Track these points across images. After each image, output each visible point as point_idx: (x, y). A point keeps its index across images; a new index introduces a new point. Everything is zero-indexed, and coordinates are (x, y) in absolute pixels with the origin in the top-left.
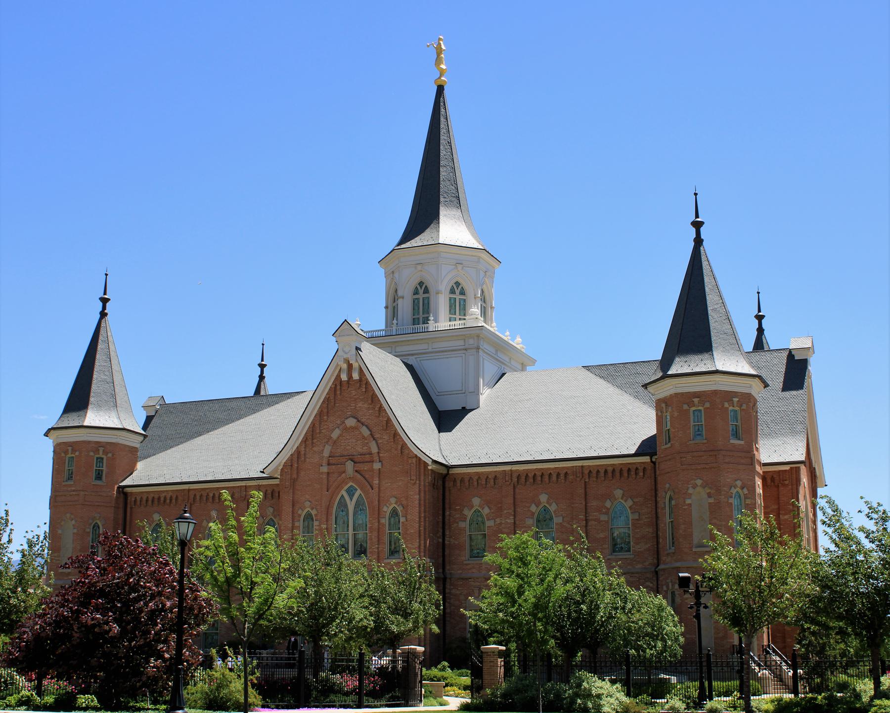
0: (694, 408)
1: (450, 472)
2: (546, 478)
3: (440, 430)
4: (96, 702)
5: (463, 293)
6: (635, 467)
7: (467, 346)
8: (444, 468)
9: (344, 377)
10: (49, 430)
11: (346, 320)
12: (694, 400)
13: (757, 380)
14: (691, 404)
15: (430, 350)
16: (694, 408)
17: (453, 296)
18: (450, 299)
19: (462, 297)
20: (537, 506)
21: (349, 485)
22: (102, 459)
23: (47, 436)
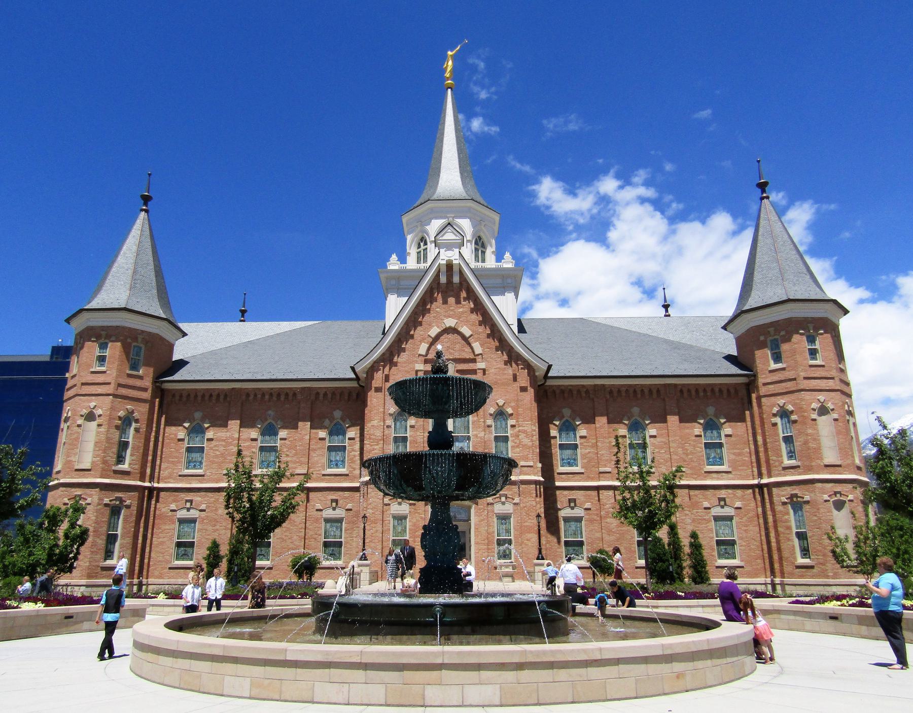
0: (771, 338)
2: (282, 398)
3: (53, 347)
4: (738, 586)
6: (216, 393)
9: (443, 279)
12: (769, 330)
13: (165, 323)
14: (135, 339)
16: (771, 338)
20: (331, 422)
22: (140, 348)
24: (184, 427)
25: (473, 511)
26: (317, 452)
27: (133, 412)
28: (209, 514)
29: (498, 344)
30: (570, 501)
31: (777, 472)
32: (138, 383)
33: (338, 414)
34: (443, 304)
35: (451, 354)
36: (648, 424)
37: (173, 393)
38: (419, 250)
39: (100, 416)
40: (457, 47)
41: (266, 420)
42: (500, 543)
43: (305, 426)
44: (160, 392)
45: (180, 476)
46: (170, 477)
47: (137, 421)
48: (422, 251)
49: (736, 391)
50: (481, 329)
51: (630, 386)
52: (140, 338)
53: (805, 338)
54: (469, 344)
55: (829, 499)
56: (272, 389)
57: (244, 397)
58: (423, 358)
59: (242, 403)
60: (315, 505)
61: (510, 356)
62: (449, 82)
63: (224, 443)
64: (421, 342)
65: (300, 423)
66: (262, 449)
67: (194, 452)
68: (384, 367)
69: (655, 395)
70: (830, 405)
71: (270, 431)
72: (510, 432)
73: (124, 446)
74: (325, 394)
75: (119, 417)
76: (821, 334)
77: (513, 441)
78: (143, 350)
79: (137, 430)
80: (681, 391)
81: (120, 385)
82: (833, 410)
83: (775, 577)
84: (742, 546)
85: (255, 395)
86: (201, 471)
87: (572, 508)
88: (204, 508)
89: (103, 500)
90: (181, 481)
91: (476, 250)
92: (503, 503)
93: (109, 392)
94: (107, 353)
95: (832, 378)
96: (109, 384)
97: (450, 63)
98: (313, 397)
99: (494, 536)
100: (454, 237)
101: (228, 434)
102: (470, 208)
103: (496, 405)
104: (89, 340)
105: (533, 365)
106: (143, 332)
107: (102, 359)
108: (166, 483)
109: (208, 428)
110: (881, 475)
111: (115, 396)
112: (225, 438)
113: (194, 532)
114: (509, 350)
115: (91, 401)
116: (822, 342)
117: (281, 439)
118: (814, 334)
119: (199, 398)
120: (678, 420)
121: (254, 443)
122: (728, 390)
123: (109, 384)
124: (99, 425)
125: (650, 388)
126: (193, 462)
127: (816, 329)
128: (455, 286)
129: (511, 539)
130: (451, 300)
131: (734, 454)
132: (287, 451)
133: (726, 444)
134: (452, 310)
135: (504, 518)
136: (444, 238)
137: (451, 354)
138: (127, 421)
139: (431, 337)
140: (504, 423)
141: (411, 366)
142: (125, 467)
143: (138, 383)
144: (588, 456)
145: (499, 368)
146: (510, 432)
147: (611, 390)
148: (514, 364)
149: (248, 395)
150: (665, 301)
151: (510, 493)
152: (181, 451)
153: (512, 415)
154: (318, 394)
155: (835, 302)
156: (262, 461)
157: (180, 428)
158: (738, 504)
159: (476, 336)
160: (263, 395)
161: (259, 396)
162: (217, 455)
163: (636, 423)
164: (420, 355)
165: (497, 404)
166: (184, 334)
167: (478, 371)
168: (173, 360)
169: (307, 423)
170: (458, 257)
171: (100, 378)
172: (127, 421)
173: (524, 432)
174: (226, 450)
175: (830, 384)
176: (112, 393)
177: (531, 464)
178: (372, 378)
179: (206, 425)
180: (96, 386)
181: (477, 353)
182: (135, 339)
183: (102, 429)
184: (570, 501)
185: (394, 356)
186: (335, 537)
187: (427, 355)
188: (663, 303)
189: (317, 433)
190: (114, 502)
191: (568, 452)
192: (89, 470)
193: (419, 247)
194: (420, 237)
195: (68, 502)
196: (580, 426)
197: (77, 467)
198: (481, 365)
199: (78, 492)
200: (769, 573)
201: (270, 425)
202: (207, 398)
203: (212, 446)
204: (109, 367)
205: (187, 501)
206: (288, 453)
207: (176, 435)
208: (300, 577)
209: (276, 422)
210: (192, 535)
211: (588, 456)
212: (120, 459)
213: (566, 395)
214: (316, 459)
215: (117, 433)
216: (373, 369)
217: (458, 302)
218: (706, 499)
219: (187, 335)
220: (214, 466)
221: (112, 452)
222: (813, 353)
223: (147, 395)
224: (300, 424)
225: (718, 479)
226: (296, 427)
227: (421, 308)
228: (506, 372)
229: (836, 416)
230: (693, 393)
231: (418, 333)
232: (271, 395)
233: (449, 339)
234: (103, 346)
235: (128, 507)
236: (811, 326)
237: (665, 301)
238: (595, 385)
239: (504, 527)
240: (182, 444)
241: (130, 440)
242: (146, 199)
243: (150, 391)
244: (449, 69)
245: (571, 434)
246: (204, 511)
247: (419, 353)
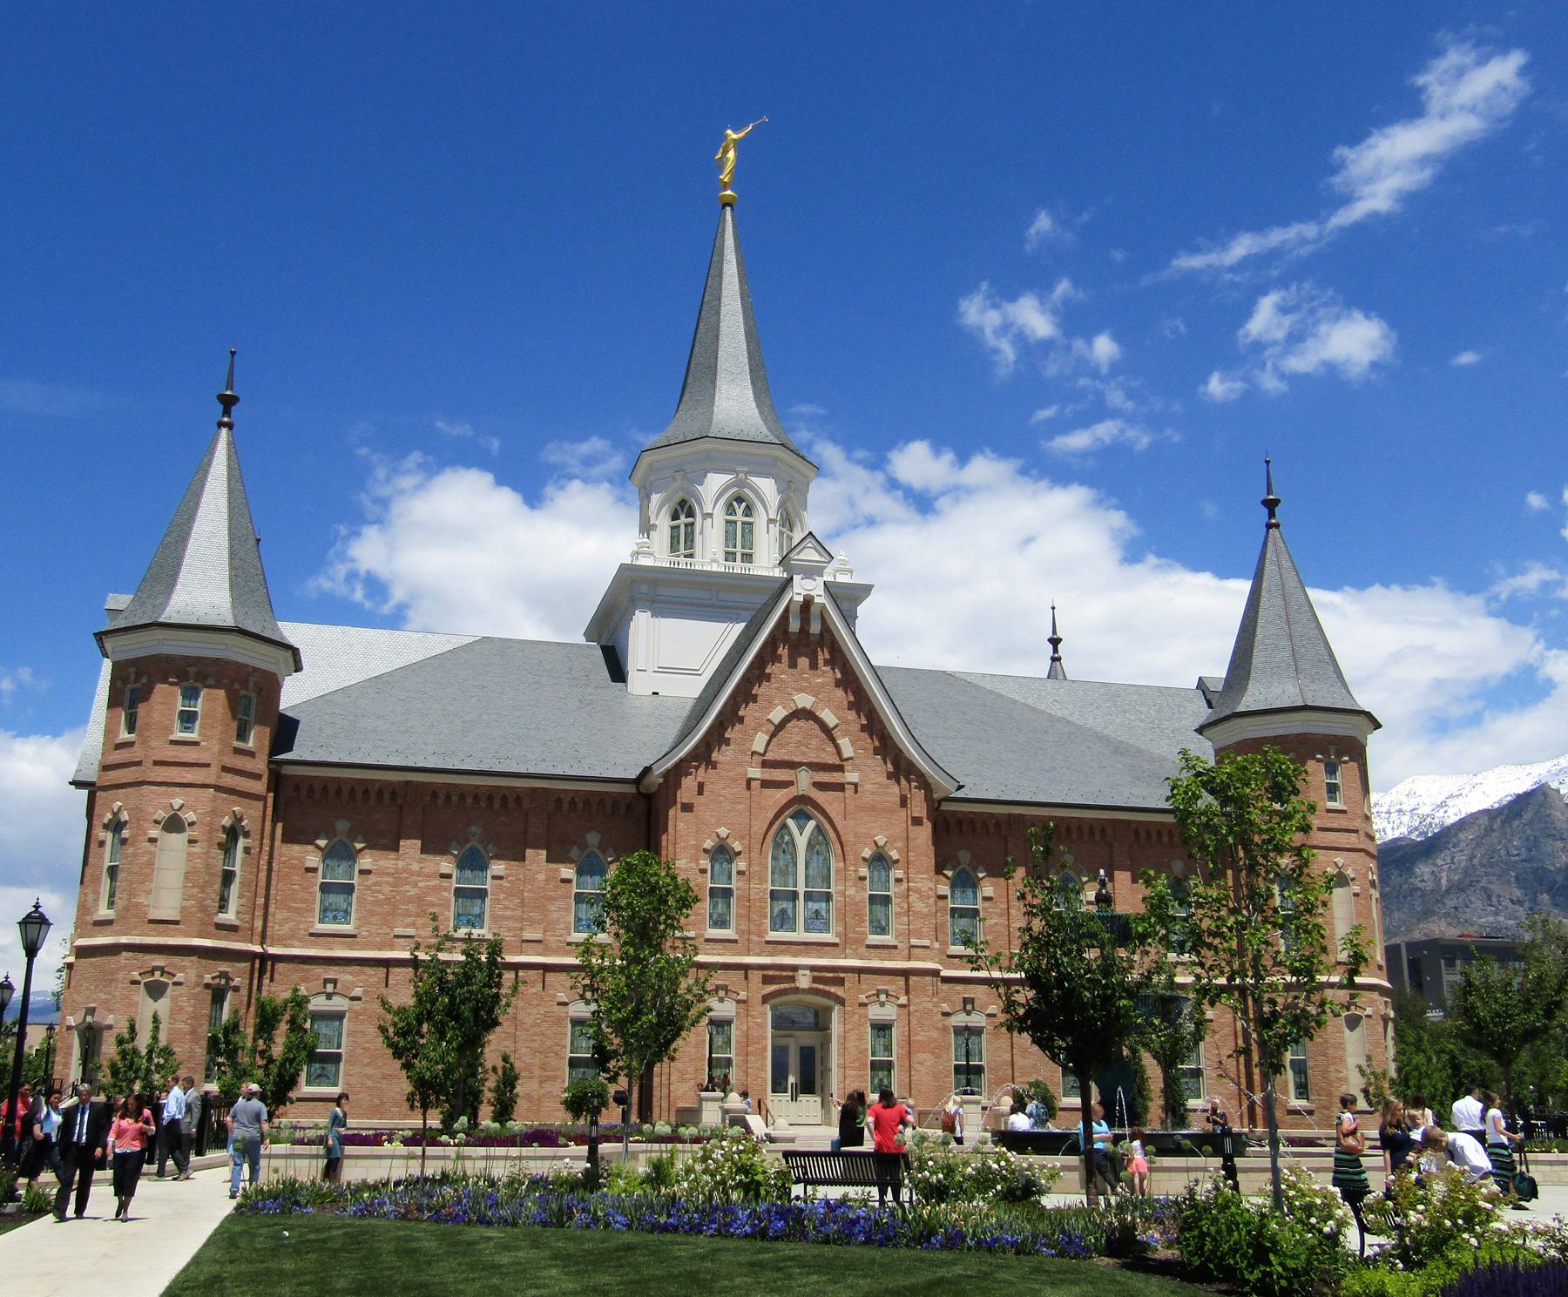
2: (497, 805)
6: (377, 787)
24: (318, 847)
25: (835, 1016)
26: (557, 904)
27: (241, 819)
28: (368, 1006)
29: (877, 743)
30: (966, 1001)
33: (593, 838)
34: (790, 667)
35: (803, 753)
36: (1086, 883)
37: (297, 782)
38: (676, 522)
39: (192, 824)
40: (748, 126)
41: (467, 841)
42: (875, 1066)
43: (537, 857)
44: (277, 780)
45: (311, 935)
46: (292, 937)
47: (247, 835)
48: (682, 527)
50: (852, 715)
51: (360, 781)
52: (252, 680)
53: (1322, 766)
54: (833, 740)
58: (761, 759)
59: (424, 809)
60: (556, 996)
61: (896, 764)
62: (729, 192)
63: (390, 879)
64: (756, 730)
65: (528, 850)
66: (459, 893)
67: (333, 893)
68: (697, 768)
69: (1098, 837)
70: (1350, 873)
71: (473, 862)
72: (893, 890)
73: (228, 877)
74: (573, 802)
75: (223, 827)
76: (1346, 762)
77: (898, 905)
78: (254, 701)
79: (247, 850)
80: (1137, 833)
81: (225, 769)
82: (1353, 879)
83: (1255, 1126)
84: (1210, 1079)
85: (448, 796)
87: (969, 1013)
88: (359, 994)
89: (202, 977)
90: (315, 945)
91: (781, 533)
92: (882, 1004)
93: (207, 781)
94: (199, 706)
95: (1356, 831)
96: (208, 765)
97: (731, 154)
99: (867, 1056)
100: (817, 558)
101: (401, 864)
102: (776, 458)
103: (873, 845)
104: (165, 681)
105: (930, 781)
106: (255, 670)
107: (188, 718)
108: (285, 946)
109: (362, 850)
110: (1468, 1012)
111: (218, 788)
112: (393, 871)
113: (340, 1035)
114: (896, 755)
115: (173, 796)
116: (1346, 774)
117: (494, 877)
118: (1336, 761)
119: (345, 795)
120: (1130, 879)
121: (445, 883)
123: (208, 765)
124: (192, 842)
125: (1091, 825)
126: (332, 911)
127: (1339, 755)
128: (812, 638)
129: (891, 1061)
130: (803, 662)
132: (505, 899)
134: (807, 680)
135: (882, 1028)
136: (801, 557)
137: (803, 753)
138: (233, 833)
139: (773, 724)
140: (883, 873)
141: (739, 770)
142: (230, 916)
144: (995, 929)
145: (879, 783)
146: (893, 890)
148: (903, 781)
149: (435, 795)
150: (1054, 632)
151: (893, 988)
152: (311, 890)
153: (897, 861)
155: (1368, 715)
156: (459, 915)
157: (310, 847)
159: (843, 727)
162: (379, 900)
164: (753, 753)
165: (875, 843)
167: (847, 786)
169: (540, 852)
170: (822, 593)
171: (190, 755)
172: (233, 833)
173: (918, 891)
174: (398, 892)
175: (1352, 840)
176: (213, 782)
177: (926, 942)
178: (678, 785)
179: (359, 846)
180: (180, 768)
181: (845, 755)
182: (245, 683)
183: (197, 849)
184: (966, 1001)
185: (712, 751)
187: (764, 755)
188: (1050, 635)
189: (558, 870)
190: (217, 981)
191: (964, 922)
192: (176, 923)
193: (675, 517)
194: (678, 498)
195: (139, 978)
196: (984, 880)
197: (151, 917)
198: (851, 776)
199: (159, 961)
200: (1246, 1121)
201: (473, 851)
202: (359, 796)
203: (369, 883)
204: (205, 735)
205: (326, 981)
206: (506, 903)
207: (302, 860)
208: (577, 1115)
209: (485, 848)
210: (336, 1040)
211: (995, 929)
212: (223, 905)
213: (965, 828)
214: (556, 915)
215: (220, 854)
216: (679, 770)
217: (814, 666)
220: (374, 919)
221: (214, 891)
222: (1332, 790)
224: (529, 852)
226: (521, 858)
227: (756, 672)
228: (889, 790)
229: (1356, 889)
231: (748, 712)
232: (476, 797)
233: (801, 727)
234: (191, 695)
235: (236, 989)
236: (1332, 749)
237: (1054, 632)
238: (1010, 815)
239: (882, 1041)
240: (313, 877)
241: (237, 868)
242: (228, 402)
243: (265, 780)
244: (729, 166)
245: (970, 893)
246: (359, 999)
247: (754, 749)
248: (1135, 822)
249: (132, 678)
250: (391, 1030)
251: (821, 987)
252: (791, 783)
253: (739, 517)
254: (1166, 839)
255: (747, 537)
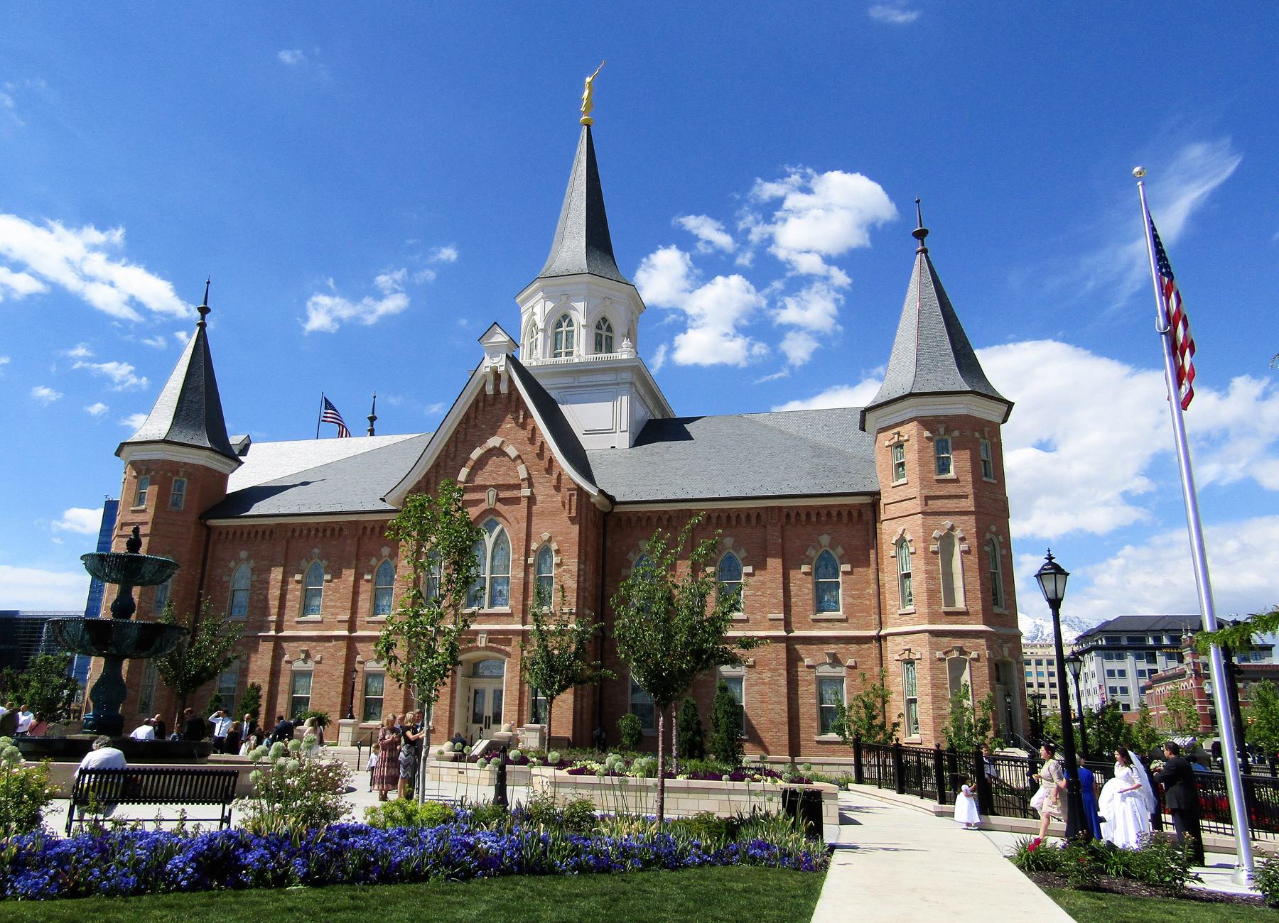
0: (177, 478)
1: (615, 510)
2: (328, 533)
5: (609, 329)
7: (619, 381)
8: (606, 502)
9: (490, 390)
10: (123, 445)
11: (495, 323)
14: (177, 473)
15: (576, 384)
16: (177, 478)
17: (599, 332)
18: (597, 335)
19: (609, 334)
21: (487, 519)
23: (119, 456)
31: (893, 621)
32: (952, 490)
35: (494, 479)
49: (860, 514)
51: (723, 510)
55: (943, 656)
56: (318, 523)
57: (290, 534)
74: (373, 529)
78: (185, 484)
80: (788, 515)
81: (927, 498)
86: (912, 607)
98: (360, 532)
106: (185, 464)
122: (850, 513)
125: (748, 513)
131: (852, 596)
133: (843, 583)
137: (494, 479)
143: (952, 490)
147: (629, 518)
154: (365, 528)
158: (850, 662)
160: (309, 530)
161: (305, 532)
163: (730, 558)
166: (243, 463)
167: (522, 499)
168: (229, 491)
182: (177, 473)
186: (376, 693)
218: (810, 654)
219: (865, 431)
223: (969, 504)
225: (828, 629)
230: (803, 517)
243: (971, 498)
248: (786, 507)
249: (143, 472)
250: (681, 638)
251: (495, 645)
252: (483, 500)
253: (604, 333)
254: (814, 519)
255: (570, 341)
